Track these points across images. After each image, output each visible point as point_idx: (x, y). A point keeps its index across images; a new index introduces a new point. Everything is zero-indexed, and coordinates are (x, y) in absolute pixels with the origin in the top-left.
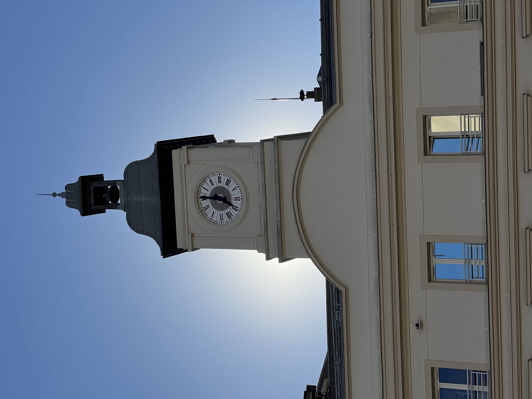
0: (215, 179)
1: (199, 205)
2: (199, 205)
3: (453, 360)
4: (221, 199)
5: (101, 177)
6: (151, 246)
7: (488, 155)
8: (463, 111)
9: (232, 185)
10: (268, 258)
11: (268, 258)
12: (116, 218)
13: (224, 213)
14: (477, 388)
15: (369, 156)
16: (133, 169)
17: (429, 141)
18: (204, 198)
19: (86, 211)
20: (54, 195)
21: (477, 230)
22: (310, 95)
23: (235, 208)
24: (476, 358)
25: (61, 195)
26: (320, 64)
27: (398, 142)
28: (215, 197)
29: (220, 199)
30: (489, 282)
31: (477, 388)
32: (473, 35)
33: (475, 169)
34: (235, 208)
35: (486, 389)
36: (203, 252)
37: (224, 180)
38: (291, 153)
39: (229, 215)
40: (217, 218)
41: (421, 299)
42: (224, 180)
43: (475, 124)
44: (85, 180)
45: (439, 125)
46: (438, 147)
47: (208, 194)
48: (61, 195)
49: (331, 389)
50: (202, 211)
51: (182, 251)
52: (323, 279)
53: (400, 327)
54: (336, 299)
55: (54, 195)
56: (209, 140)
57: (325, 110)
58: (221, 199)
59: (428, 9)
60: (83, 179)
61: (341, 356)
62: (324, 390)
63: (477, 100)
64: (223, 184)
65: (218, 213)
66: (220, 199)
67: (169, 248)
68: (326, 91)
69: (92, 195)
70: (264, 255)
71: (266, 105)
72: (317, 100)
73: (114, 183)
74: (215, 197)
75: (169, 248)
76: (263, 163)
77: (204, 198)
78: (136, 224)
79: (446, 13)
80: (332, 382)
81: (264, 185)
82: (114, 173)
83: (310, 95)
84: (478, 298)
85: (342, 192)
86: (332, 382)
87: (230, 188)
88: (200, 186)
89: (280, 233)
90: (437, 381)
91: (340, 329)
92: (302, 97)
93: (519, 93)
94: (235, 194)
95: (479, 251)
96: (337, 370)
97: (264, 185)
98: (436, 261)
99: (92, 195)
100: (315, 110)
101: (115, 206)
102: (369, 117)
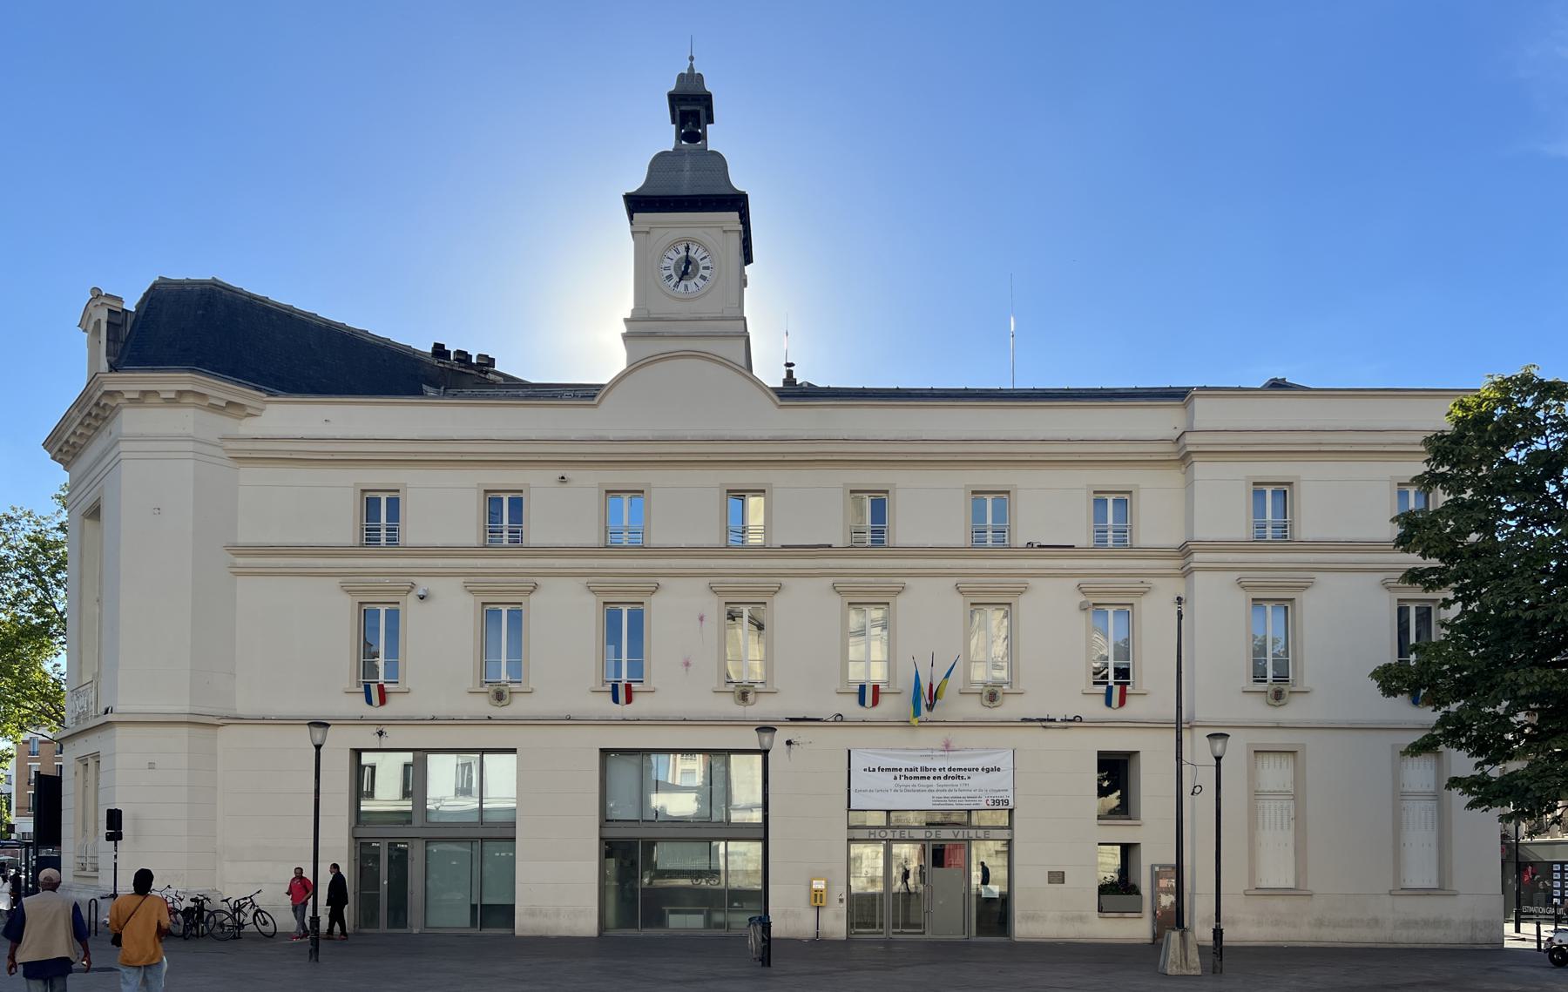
0: (706, 263)
1: (680, 242)
2: (680, 242)
3: (530, 511)
4: (687, 269)
5: (710, 120)
6: (635, 181)
7: (726, 550)
8: (768, 528)
9: (701, 283)
10: (626, 320)
11: (626, 320)
12: (665, 137)
13: (672, 272)
14: (506, 533)
15: (727, 434)
16: (718, 161)
17: (740, 494)
18: (687, 249)
19: (674, 98)
20: (692, 58)
21: (656, 539)
22: (790, 373)
23: (676, 285)
24: (535, 532)
25: (691, 68)
26: (632, 306)
27: (739, 462)
28: (688, 261)
29: (686, 268)
30: (608, 549)
31: (506, 533)
32: (838, 539)
33: (713, 538)
34: (676, 285)
35: (506, 543)
36: (629, 244)
37: (706, 273)
38: (732, 350)
39: (669, 277)
40: (667, 263)
41: (589, 481)
42: (706, 273)
43: (755, 539)
44: (707, 98)
45: (755, 504)
46: (735, 504)
47: (691, 254)
48: (691, 68)
49: (493, 384)
50: (673, 246)
51: (631, 218)
52: (605, 382)
53: (563, 460)
54: (586, 394)
55: (692, 58)
56: (748, 259)
57: (775, 390)
58: (687, 269)
59: (866, 496)
60: (708, 97)
61: (527, 397)
62: (491, 376)
63: (777, 542)
64: (702, 272)
65: (672, 264)
66: (686, 268)
67: (636, 203)
68: (793, 392)
69: (691, 109)
70: (628, 316)
71: (786, 322)
72: (785, 382)
73: (703, 137)
74: (688, 261)
75: (636, 203)
76: (723, 319)
77: (687, 249)
78: (660, 162)
79: (861, 513)
80: (500, 386)
81: (700, 319)
82: (716, 138)
83: (790, 373)
84: (593, 538)
85: (691, 406)
86: (500, 386)
87: (697, 280)
88: (700, 245)
89: (652, 335)
90: (387, 607)
91: (554, 397)
92: (789, 365)
93: (782, 580)
94: (691, 284)
95: (638, 539)
96: (513, 391)
97: (700, 319)
98: (626, 497)
99: (691, 109)
100: (777, 381)
101: (680, 137)
102: (766, 435)
